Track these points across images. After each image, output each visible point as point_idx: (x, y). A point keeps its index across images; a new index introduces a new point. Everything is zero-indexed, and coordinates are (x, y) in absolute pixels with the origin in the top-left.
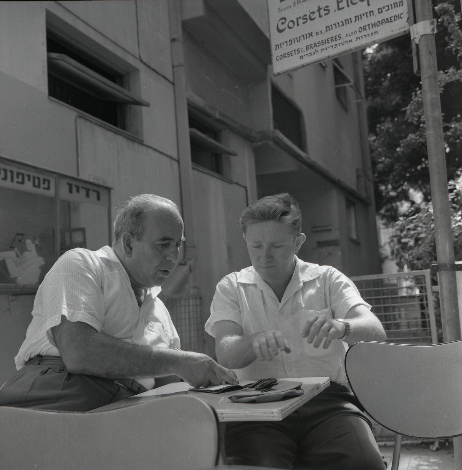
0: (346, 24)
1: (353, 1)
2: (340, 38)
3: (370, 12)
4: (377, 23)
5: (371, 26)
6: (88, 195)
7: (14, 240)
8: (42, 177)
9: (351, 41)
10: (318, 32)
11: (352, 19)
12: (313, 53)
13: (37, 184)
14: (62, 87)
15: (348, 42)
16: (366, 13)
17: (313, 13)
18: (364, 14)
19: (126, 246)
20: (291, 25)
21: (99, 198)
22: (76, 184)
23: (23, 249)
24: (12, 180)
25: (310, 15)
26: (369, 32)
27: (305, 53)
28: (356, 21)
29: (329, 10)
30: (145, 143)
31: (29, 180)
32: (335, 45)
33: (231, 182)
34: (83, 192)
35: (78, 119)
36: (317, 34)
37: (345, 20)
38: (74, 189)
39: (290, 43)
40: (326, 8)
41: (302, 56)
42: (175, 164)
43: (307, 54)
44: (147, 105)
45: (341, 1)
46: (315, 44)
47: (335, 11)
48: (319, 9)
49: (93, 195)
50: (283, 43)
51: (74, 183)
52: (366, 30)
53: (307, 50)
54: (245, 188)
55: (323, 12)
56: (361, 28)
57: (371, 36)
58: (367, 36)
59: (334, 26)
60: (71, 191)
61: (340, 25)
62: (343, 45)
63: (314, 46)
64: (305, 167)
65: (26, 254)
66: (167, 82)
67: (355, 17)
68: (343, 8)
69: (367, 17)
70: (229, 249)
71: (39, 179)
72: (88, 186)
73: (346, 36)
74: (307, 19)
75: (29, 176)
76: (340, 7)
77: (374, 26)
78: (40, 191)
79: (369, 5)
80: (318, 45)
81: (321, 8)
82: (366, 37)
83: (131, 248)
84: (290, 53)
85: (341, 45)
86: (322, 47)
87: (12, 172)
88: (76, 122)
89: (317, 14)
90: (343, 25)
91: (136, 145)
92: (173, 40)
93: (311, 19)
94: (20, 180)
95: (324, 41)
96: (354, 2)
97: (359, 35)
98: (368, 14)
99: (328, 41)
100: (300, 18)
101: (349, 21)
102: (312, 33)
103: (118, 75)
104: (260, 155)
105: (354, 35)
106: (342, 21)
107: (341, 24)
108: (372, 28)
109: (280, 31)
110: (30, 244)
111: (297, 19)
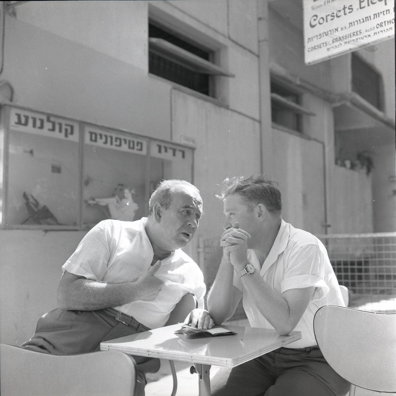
0: (366, 21)
1: (373, 1)
2: (360, 33)
3: (387, 11)
4: (392, 21)
5: (386, 23)
6: (174, 154)
7: (116, 189)
8: (136, 140)
9: (369, 36)
10: (343, 28)
11: (371, 17)
12: (337, 46)
13: (131, 146)
14: (160, 65)
15: (367, 36)
16: (383, 12)
17: (340, 11)
18: (381, 13)
19: (156, 214)
20: (321, 21)
21: (183, 156)
22: (166, 145)
23: (122, 197)
24: (112, 143)
25: (337, 13)
26: (384, 28)
27: (331, 46)
28: (374, 18)
29: (352, 9)
30: (231, 107)
31: (125, 143)
32: (356, 39)
33: (309, 138)
34: (170, 152)
35: (174, 91)
36: (342, 29)
37: (366, 18)
38: (163, 150)
39: (320, 37)
40: (350, 7)
41: (329, 48)
42: (257, 125)
43: (333, 47)
44: (233, 76)
45: (363, 1)
46: (340, 38)
47: (358, 9)
48: (344, 8)
49: (179, 154)
50: (314, 37)
51: (163, 145)
52: (382, 26)
53: (333, 43)
54: (323, 143)
55: (347, 11)
56: (378, 24)
57: (387, 31)
58: (383, 31)
59: (356, 23)
60: (160, 151)
61: (361, 22)
62: (362, 39)
63: (339, 40)
64: (383, 125)
65: (124, 200)
66: (252, 55)
67: (374, 15)
68: (364, 7)
69: (384, 14)
70: (304, 197)
71: (133, 142)
72: (175, 147)
73: (366, 31)
74: (334, 16)
75: (125, 140)
76: (362, 6)
77: (389, 23)
78: (135, 151)
79: (386, 4)
80: (342, 39)
81: (346, 8)
82: (382, 32)
83: (160, 217)
84: (319, 46)
85: (361, 39)
86: (345, 41)
87: (111, 137)
88: (171, 93)
89: (342, 12)
90: (364, 21)
91: (223, 110)
92: (260, 19)
93: (338, 17)
94: (118, 143)
95: (347, 36)
96: (374, 2)
97: (376, 30)
98: (385, 13)
99: (350, 35)
100: (329, 15)
101: (369, 18)
102: (337, 28)
103: (206, 53)
104: (339, 115)
105: (372, 30)
106: (363, 18)
107: (362, 21)
108: (388, 24)
109: (312, 26)
110: (127, 193)
111: (327, 16)
